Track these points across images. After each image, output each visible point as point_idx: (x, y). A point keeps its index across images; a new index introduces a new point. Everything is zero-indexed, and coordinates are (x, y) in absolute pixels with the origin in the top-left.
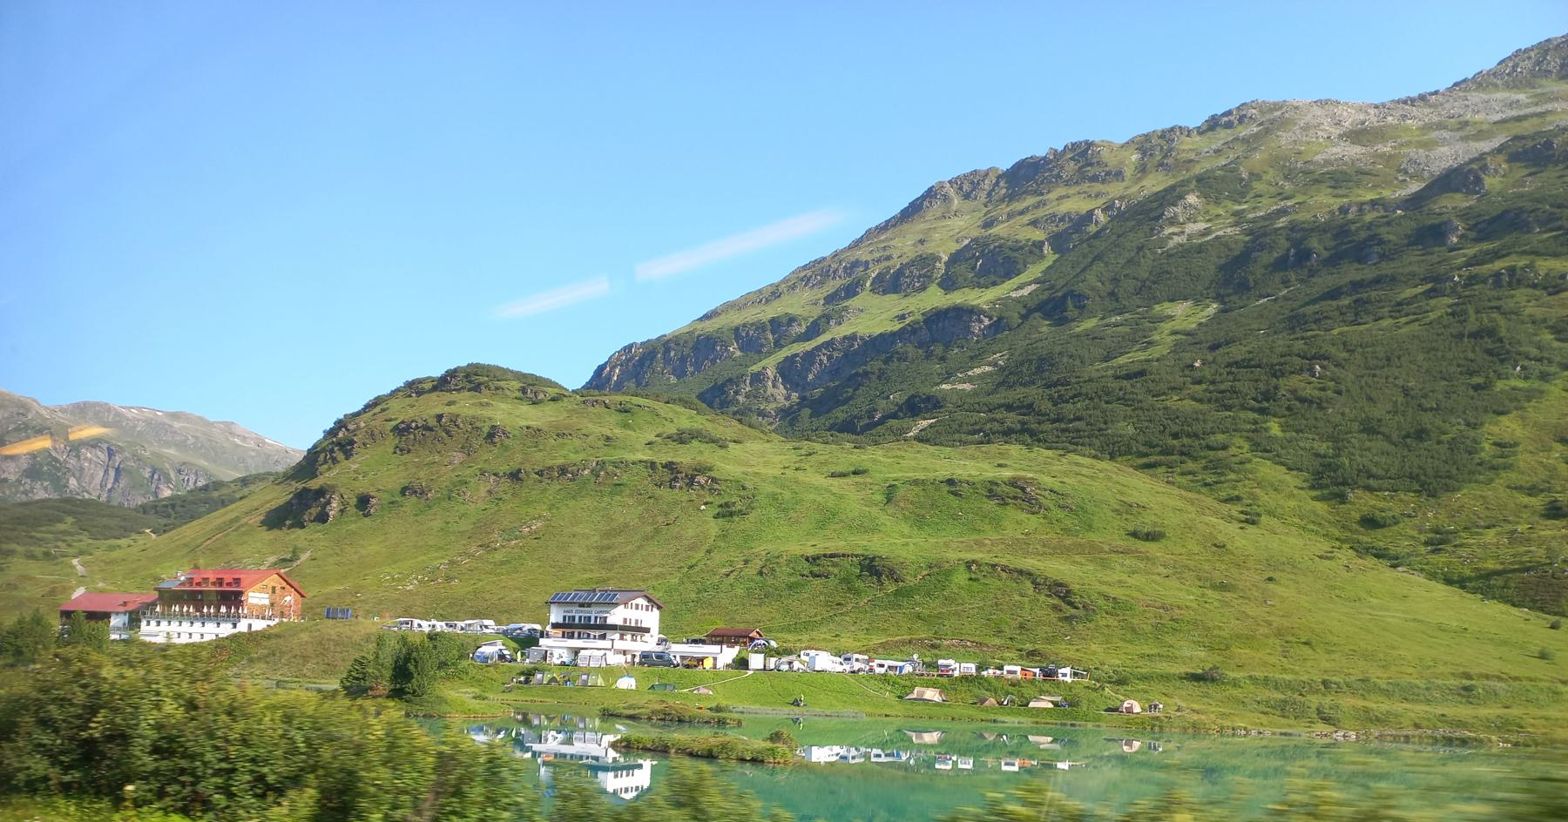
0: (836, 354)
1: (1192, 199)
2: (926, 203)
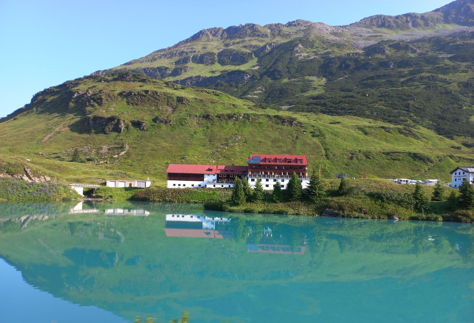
0: (193, 82)
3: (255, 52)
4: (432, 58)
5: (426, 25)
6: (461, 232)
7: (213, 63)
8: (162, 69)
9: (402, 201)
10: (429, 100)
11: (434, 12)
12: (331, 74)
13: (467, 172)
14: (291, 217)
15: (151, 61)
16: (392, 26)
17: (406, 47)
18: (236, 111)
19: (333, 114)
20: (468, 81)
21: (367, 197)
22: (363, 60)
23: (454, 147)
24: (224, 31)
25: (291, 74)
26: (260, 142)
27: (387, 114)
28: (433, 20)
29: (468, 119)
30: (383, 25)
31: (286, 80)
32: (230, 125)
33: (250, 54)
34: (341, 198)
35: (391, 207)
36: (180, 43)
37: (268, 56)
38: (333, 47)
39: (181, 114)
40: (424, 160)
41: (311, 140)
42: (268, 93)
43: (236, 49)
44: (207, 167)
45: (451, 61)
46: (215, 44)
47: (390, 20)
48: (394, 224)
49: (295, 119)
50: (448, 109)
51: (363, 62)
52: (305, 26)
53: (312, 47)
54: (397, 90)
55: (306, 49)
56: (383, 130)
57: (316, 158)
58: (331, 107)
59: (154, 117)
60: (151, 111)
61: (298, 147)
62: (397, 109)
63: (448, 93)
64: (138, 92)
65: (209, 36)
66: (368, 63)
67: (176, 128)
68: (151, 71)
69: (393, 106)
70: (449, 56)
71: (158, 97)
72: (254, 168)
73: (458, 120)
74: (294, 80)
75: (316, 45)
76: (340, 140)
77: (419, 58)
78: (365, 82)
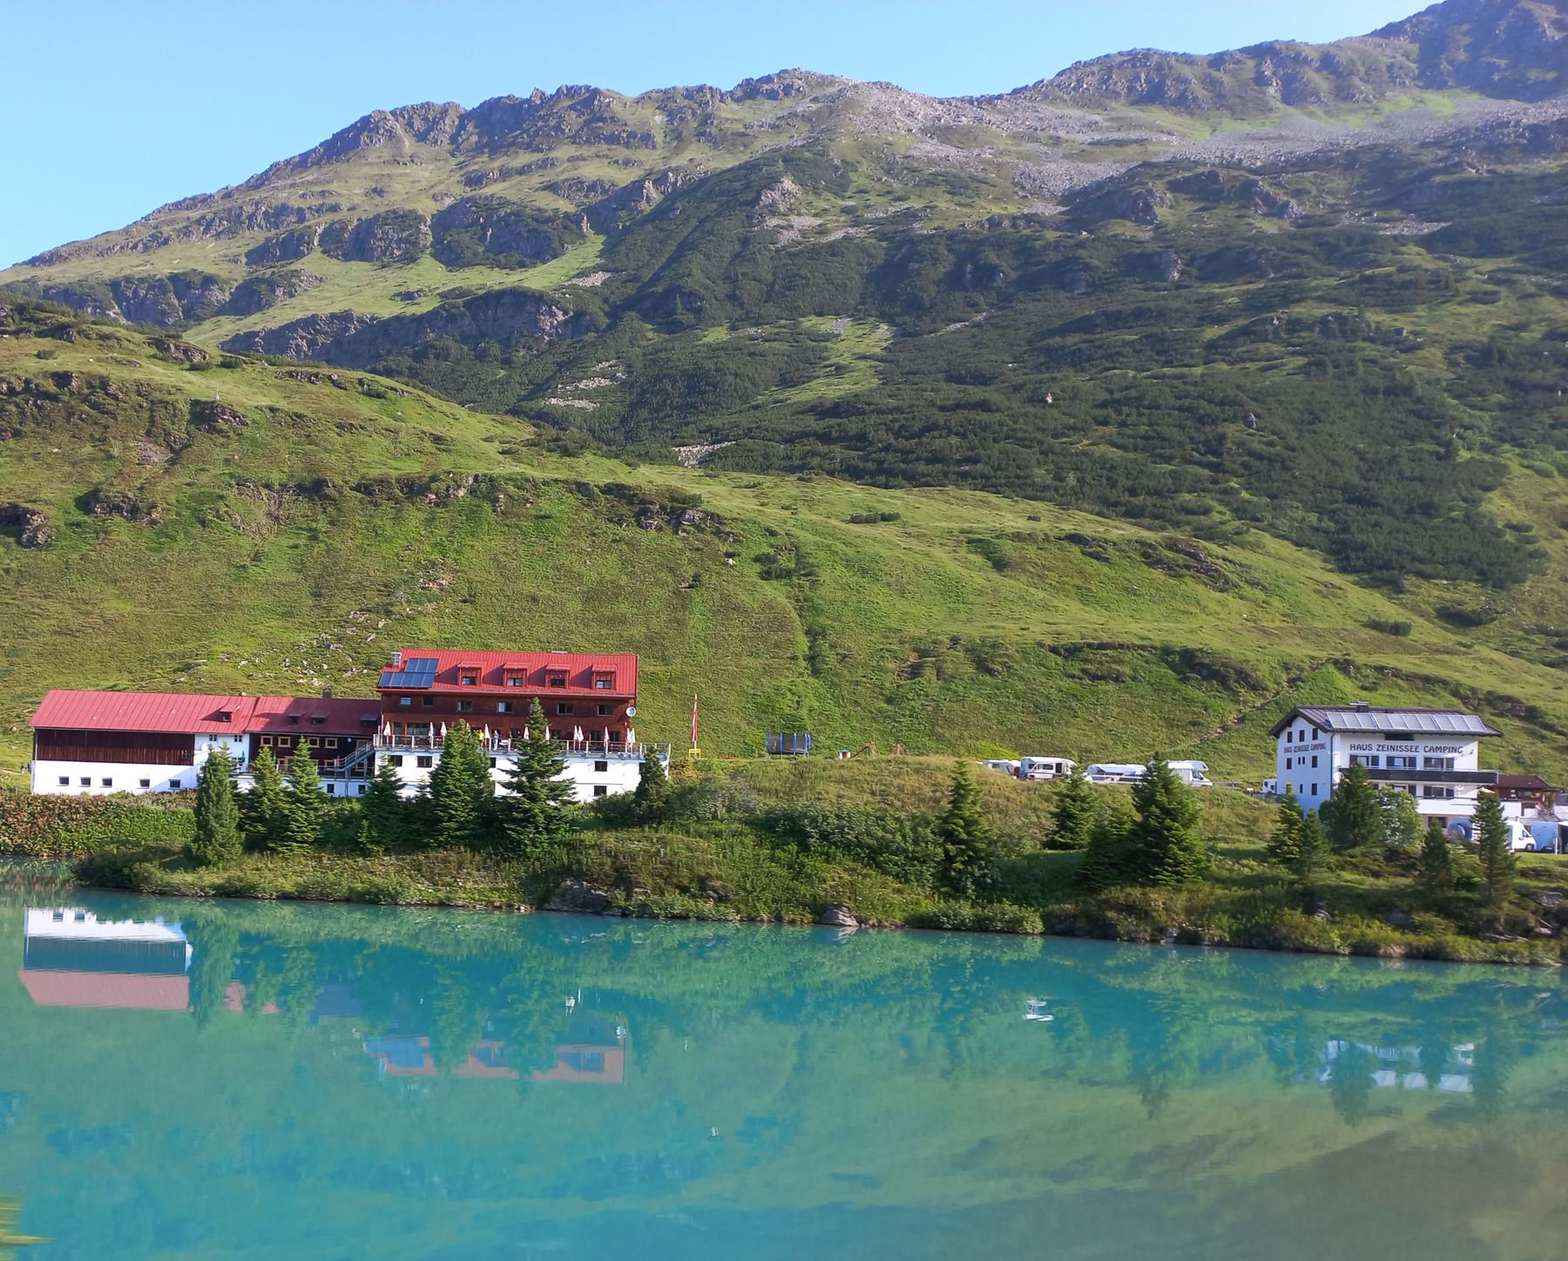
1: (788, 184)
2: (364, 138)
3: (593, 213)
4: (1349, 240)
5: (1344, 93)
6: (1117, 981)
7: (410, 259)
8: (189, 285)
9: (885, 847)
10: (1311, 423)
11: (1378, 40)
12: (916, 306)
13: (1326, 728)
14: (421, 918)
15: (146, 248)
16: (1195, 99)
17: (1245, 193)
18: (446, 462)
19: (892, 481)
20: (1492, 338)
21: (746, 829)
22: (1056, 246)
23: (1377, 626)
24: (465, 117)
25: (741, 305)
26: (534, 599)
27: (1123, 482)
28: (1371, 71)
29: (1475, 502)
30: (1154, 96)
31: (717, 335)
32: (412, 524)
33: (572, 220)
34: (636, 833)
35: (833, 875)
36: (276, 170)
37: (649, 227)
38: (929, 190)
39: (204, 478)
40: (1223, 681)
41: (752, 591)
42: (637, 390)
43: (511, 195)
44: (213, 704)
45: (1431, 250)
46: (425, 174)
47: (1187, 72)
48: (838, 944)
49: (695, 501)
50: (1393, 460)
51: (1052, 257)
52: (815, 100)
53: (840, 188)
54: (1177, 377)
55: (811, 198)
56: (1076, 549)
57: (767, 671)
58: (886, 449)
59: (83, 490)
60: (74, 464)
61: (696, 621)
62: (1168, 460)
63: (1397, 390)
64: (27, 382)
65: (399, 140)
66: (1076, 259)
67: (174, 539)
68: (142, 293)
69: (1154, 445)
70: (1427, 228)
71: (110, 404)
72: (404, 710)
73: (1428, 509)
74: (752, 331)
75: (858, 180)
76: (878, 595)
77: (1292, 237)
78: (1055, 341)
